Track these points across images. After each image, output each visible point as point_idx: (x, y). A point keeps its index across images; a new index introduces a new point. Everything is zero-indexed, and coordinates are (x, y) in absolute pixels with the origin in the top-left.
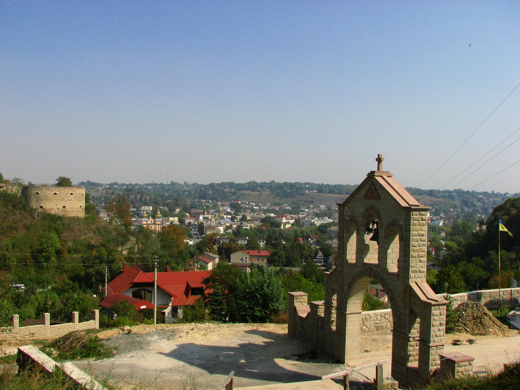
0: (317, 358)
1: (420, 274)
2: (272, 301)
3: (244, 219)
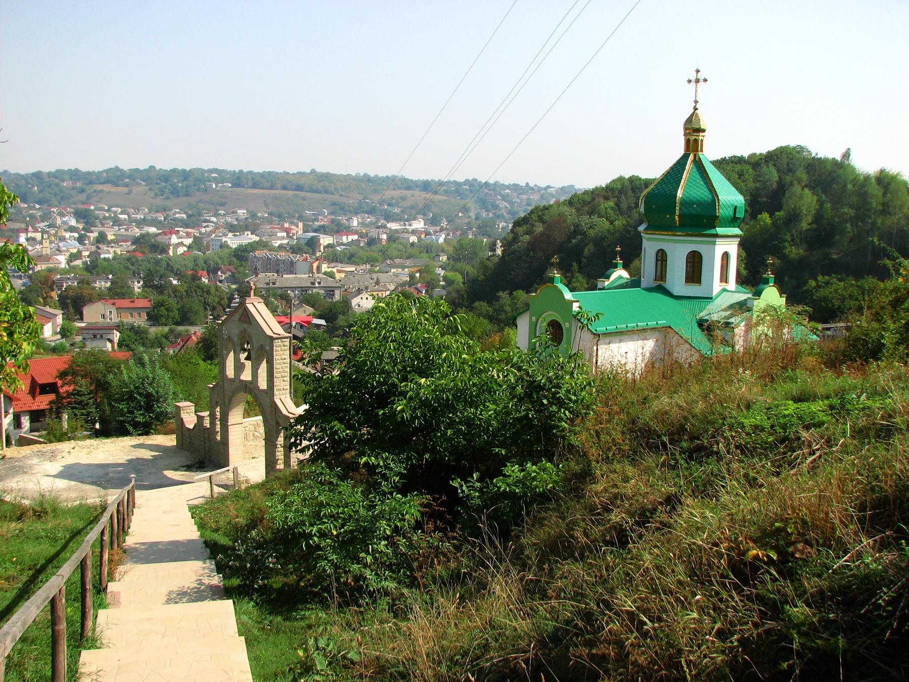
0: (204, 468)
1: (284, 392)
2: (158, 401)
3: (102, 239)
